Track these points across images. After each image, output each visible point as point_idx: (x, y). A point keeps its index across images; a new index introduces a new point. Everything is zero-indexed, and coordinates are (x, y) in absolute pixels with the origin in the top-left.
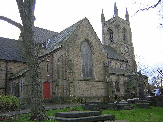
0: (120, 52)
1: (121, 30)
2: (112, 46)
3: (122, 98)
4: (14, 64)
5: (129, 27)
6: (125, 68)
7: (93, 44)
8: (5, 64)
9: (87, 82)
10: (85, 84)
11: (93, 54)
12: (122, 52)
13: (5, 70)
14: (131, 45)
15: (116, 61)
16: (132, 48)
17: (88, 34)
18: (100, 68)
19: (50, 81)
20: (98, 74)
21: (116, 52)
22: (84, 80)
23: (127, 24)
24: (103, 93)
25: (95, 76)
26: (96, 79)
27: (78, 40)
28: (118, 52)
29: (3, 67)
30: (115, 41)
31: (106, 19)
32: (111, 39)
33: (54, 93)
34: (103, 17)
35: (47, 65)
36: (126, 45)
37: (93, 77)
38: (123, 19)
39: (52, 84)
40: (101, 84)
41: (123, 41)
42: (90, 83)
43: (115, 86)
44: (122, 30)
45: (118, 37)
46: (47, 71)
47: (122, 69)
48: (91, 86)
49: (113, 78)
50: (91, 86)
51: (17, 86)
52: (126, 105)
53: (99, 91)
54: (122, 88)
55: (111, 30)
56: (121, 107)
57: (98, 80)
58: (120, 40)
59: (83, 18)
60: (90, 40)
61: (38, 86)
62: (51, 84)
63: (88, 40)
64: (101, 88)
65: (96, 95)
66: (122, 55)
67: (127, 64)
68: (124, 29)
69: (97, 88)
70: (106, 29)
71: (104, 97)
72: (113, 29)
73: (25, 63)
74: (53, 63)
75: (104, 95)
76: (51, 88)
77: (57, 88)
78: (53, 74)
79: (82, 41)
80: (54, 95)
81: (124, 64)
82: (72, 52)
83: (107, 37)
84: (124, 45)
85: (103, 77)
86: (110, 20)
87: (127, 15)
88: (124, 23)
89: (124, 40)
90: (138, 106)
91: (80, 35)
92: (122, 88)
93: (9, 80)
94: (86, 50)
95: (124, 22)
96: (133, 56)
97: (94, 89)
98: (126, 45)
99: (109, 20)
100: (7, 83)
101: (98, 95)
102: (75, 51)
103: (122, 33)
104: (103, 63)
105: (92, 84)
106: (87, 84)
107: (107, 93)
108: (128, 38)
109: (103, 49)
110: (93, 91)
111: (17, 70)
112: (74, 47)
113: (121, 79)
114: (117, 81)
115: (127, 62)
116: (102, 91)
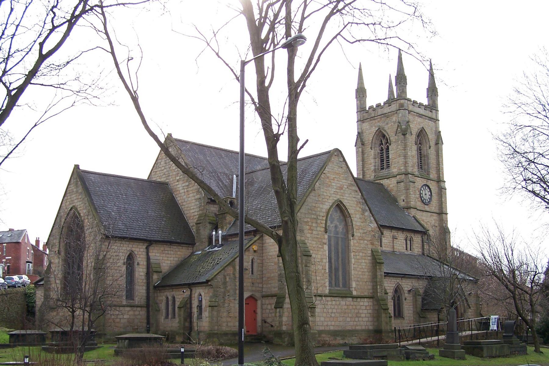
0: (408, 202)
1: (411, 139)
2: (385, 182)
3: (183, 170)
4: (162, 249)
5: (437, 127)
6: (417, 250)
7: (351, 211)
8: (145, 250)
9: (337, 299)
10: (334, 303)
11: (350, 236)
12: (412, 204)
13: (145, 263)
14: (440, 181)
15: (395, 233)
16: (441, 191)
17: (341, 188)
18: (364, 267)
19: (257, 295)
20: (359, 279)
21: (394, 200)
22: (331, 295)
23: (431, 119)
24: (369, 323)
25: (354, 285)
26: (355, 293)
27: (321, 206)
28: (402, 204)
29: (141, 256)
30: (394, 170)
31: (371, 101)
32: (382, 161)
33: (265, 322)
34: (361, 93)
35: (252, 260)
36: (425, 182)
37: (349, 288)
38: (421, 105)
39: (262, 301)
40: (366, 303)
41: (416, 171)
42: (343, 302)
43: (392, 304)
44: (414, 136)
45: (401, 160)
46: (252, 273)
47: (409, 252)
48: (346, 307)
49: (389, 285)
50: (346, 307)
51: (187, 304)
52: (420, 353)
53: (360, 319)
54: (408, 309)
55: (384, 136)
56: (411, 356)
57: (359, 294)
58: (410, 170)
59: (331, 148)
60: (345, 202)
61: (308, 326)
62: (259, 302)
63: (342, 203)
64: (366, 311)
65: (354, 328)
66: (413, 212)
67: (425, 240)
68: (421, 134)
69: (356, 311)
70: (370, 131)
71: (369, 331)
72: (390, 130)
73: (185, 245)
74: (264, 255)
75: (371, 328)
76: (259, 311)
77: (280, 312)
78: (264, 279)
79: (328, 207)
80: (265, 325)
81: (417, 239)
82: (309, 235)
83: (372, 154)
84: (420, 182)
85: (370, 287)
86: (382, 108)
87: (432, 91)
88: (420, 115)
89: (421, 167)
90: (443, 355)
91: (325, 194)
92: (408, 309)
93: (155, 287)
94: (336, 227)
95: (424, 114)
96: (442, 213)
97: (350, 315)
98: (425, 182)
99: (378, 105)
100: (151, 294)
101: (357, 328)
102: (314, 232)
103: (415, 148)
104: (370, 255)
105: (348, 303)
106: (338, 303)
107: (376, 324)
108: (432, 161)
109: (371, 222)
110: (348, 319)
111: (169, 262)
112: (312, 223)
113: (407, 285)
114: (397, 290)
115: (424, 233)
116: (366, 319)
